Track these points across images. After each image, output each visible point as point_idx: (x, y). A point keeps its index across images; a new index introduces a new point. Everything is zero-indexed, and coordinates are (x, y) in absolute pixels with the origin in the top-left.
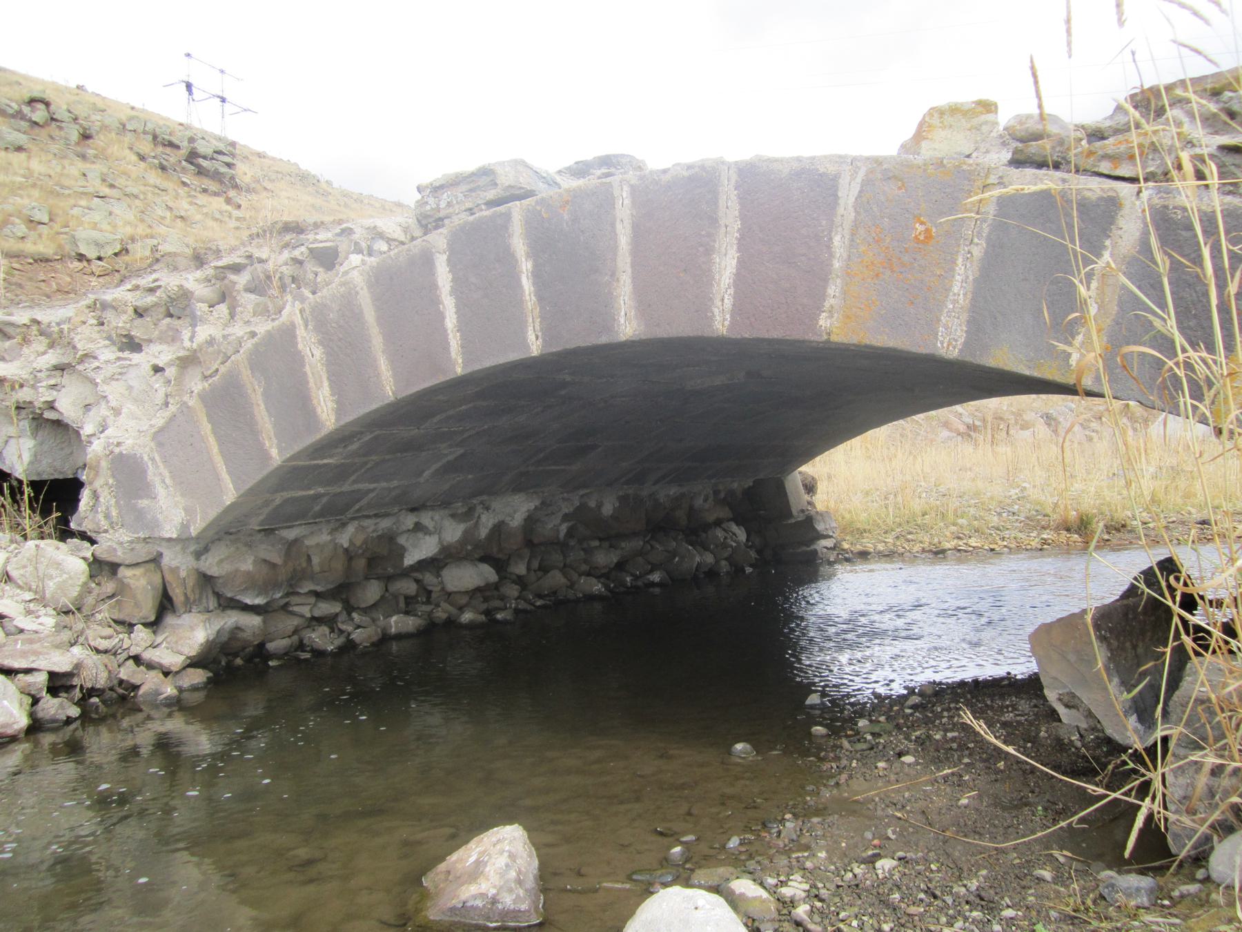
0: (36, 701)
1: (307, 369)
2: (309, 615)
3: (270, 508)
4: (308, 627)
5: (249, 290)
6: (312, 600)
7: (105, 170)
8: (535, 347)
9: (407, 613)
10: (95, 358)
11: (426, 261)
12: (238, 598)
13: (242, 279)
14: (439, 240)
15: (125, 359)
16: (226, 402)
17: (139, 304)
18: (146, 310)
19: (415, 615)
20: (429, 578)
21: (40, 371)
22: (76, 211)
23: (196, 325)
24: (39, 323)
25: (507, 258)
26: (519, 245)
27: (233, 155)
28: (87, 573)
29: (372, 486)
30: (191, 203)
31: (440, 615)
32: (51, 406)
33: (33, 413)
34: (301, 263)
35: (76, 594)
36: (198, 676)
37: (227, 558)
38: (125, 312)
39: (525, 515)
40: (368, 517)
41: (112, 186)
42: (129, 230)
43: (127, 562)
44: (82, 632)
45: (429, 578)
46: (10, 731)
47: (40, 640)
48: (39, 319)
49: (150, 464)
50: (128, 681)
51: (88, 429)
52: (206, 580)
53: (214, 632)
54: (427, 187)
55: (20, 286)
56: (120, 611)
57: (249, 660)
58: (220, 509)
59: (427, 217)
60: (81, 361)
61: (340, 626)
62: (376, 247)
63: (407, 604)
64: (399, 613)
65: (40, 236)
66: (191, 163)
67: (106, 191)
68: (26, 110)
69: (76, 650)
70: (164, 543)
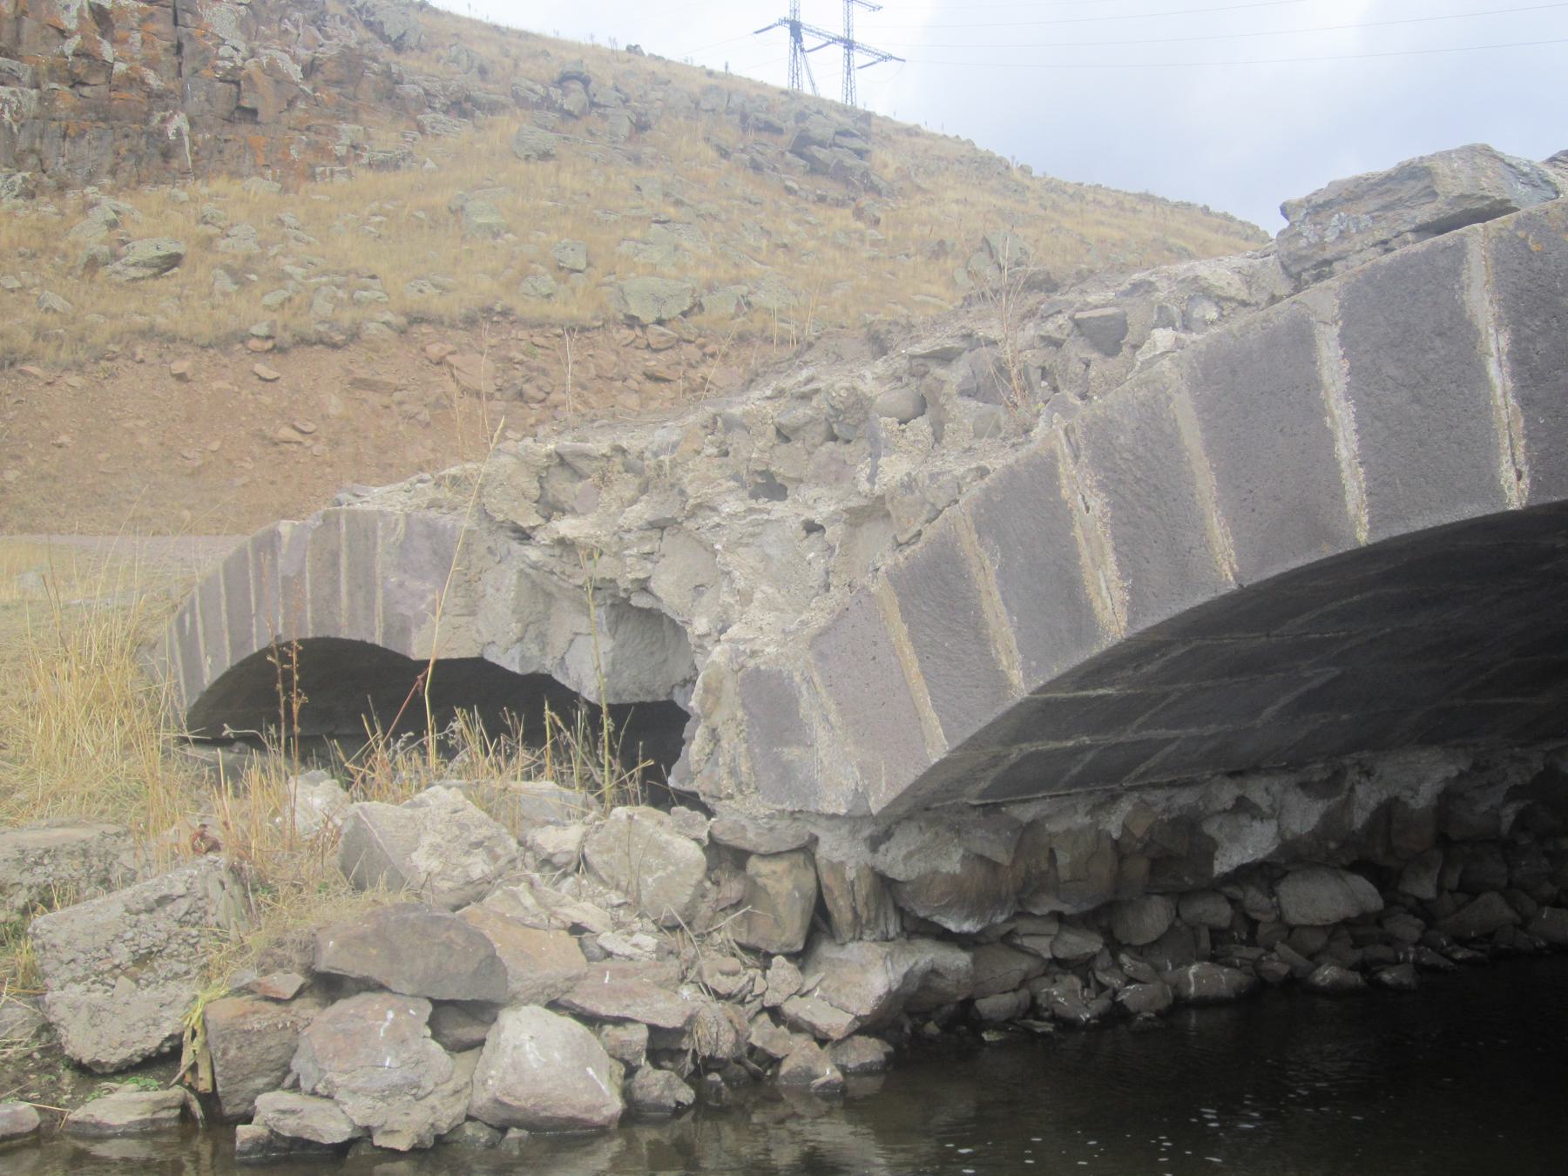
0: (631, 1071)
1: (1078, 532)
2: (1048, 955)
3: (999, 770)
4: (1045, 974)
5: (966, 393)
6: (1054, 928)
7: (668, 178)
8: (1515, 494)
9: (1213, 959)
10: (714, 509)
11: (1301, 336)
12: (936, 919)
13: (954, 376)
14: (1324, 300)
15: (761, 511)
16: (935, 588)
17: (783, 420)
18: (796, 430)
19: (1230, 965)
20: (1254, 898)
21: (629, 531)
22: (625, 248)
23: (878, 456)
24: (624, 451)
25: (1460, 331)
26: (1481, 302)
27: (866, 136)
28: (704, 866)
29: (1174, 733)
30: (799, 222)
31: (1278, 965)
32: (643, 586)
33: (614, 596)
34: (1058, 344)
35: (686, 899)
36: (870, 1051)
37: (920, 850)
38: (762, 435)
39: (1440, 788)
40: (1155, 786)
41: (678, 203)
42: (704, 273)
43: (762, 850)
44: (691, 964)
45: (1254, 898)
46: (597, 1119)
47: (637, 972)
48: (625, 445)
49: (804, 688)
50: (763, 1050)
51: (700, 625)
52: (885, 885)
53: (899, 978)
54: (1300, 205)
55: (544, 372)
56: (749, 931)
57: (947, 1027)
58: (920, 771)
59: (1301, 259)
60: (692, 515)
61: (1099, 976)
62: (1196, 314)
63: (1214, 943)
64: (1200, 958)
65: (573, 290)
66: (801, 155)
67: (672, 211)
68: (556, 93)
69: (687, 991)
70: (823, 822)
